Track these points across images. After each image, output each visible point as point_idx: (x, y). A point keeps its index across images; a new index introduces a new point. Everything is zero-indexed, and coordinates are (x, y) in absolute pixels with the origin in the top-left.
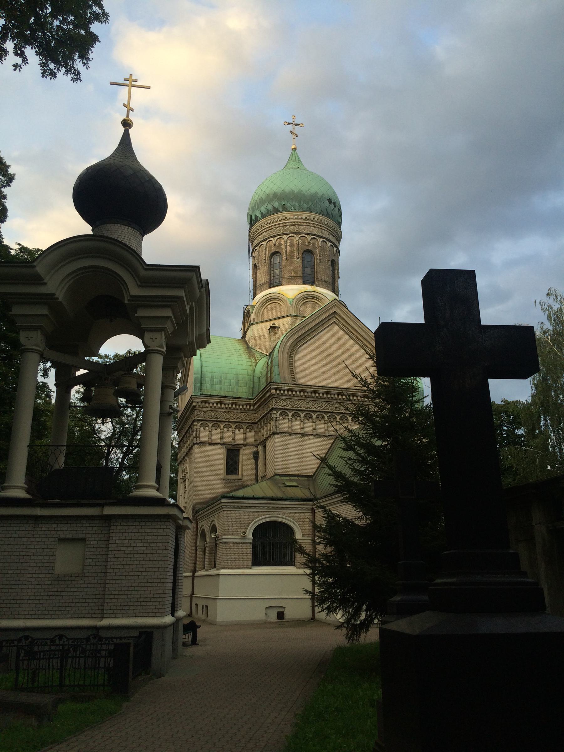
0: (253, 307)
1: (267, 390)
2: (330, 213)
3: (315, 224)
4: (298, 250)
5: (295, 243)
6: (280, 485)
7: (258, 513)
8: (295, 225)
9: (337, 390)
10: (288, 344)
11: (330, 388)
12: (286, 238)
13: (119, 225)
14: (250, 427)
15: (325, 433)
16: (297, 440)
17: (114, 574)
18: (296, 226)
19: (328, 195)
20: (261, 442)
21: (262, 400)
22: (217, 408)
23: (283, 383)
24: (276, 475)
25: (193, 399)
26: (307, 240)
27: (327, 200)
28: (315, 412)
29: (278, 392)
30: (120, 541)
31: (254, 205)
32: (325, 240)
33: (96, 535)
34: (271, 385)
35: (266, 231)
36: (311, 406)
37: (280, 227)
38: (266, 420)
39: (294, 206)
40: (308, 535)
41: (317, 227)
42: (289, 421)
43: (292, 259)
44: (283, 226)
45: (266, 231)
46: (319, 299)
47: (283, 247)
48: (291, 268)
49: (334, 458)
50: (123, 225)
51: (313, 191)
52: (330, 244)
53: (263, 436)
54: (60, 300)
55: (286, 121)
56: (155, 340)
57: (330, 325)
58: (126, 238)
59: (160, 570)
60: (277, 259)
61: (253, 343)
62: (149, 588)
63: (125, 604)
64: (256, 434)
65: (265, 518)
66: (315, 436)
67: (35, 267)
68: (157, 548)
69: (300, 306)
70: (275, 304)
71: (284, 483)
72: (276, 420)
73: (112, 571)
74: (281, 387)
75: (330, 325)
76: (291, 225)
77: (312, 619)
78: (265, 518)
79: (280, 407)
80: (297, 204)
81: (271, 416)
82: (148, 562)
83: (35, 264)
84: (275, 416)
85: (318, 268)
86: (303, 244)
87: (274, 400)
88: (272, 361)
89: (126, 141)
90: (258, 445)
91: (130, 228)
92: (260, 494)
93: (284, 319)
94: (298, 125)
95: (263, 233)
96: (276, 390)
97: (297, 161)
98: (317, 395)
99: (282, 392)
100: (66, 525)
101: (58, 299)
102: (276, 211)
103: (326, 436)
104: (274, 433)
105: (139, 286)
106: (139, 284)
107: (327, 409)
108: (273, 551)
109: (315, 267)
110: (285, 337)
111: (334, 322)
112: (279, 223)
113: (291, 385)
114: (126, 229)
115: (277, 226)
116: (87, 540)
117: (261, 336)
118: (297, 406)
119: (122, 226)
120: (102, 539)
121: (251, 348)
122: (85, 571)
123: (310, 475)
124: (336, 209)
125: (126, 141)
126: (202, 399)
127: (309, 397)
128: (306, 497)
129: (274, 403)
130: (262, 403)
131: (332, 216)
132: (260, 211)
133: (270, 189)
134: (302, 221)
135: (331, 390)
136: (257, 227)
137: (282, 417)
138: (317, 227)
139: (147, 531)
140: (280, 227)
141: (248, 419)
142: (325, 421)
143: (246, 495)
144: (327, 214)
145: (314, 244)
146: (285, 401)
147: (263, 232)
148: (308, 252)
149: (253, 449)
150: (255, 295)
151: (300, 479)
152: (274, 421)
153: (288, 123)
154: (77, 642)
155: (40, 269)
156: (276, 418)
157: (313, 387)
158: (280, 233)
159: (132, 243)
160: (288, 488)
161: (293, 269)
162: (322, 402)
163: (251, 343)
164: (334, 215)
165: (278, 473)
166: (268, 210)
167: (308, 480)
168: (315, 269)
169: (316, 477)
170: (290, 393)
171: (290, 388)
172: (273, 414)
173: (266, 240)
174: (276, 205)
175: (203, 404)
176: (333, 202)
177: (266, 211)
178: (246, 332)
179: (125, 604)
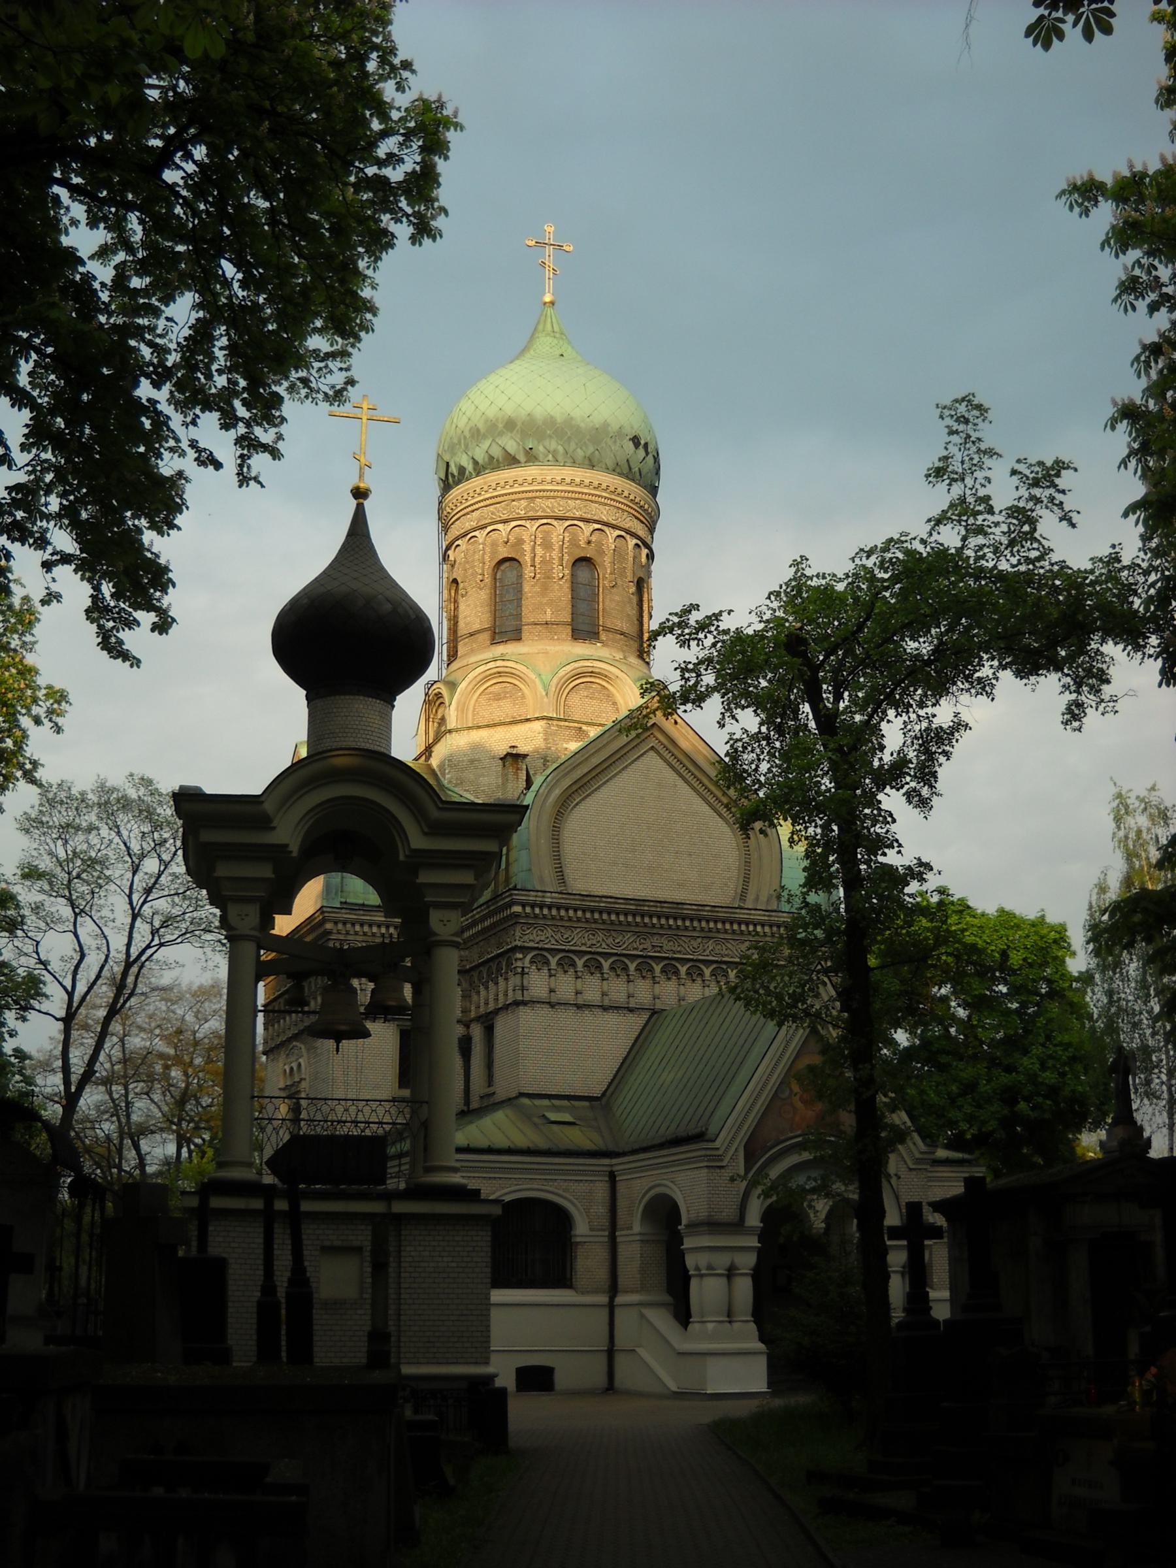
3: (602, 497)
4: (561, 559)
5: (554, 540)
6: (536, 1120)
8: (554, 498)
9: (656, 907)
11: (641, 903)
12: (535, 528)
13: (361, 698)
15: (628, 1003)
16: (567, 1017)
18: (558, 499)
20: (480, 1017)
21: (487, 923)
22: (370, 934)
24: (522, 1095)
25: (326, 915)
26: (583, 533)
28: (606, 955)
29: (528, 910)
31: (456, 441)
32: (623, 533)
34: (511, 895)
35: (486, 506)
36: (601, 942)
37: (520, 499)
39: (555, 454)
41: (606, 504)
42: (550, 976)
43: (549, 578)
44: (527, 498)
45: (486, 506)
46: (610, 678)
47: (527, 547)
48: (545, 600)
49: (649, 1064)
50: (369, 696)
51: (597, 420)
52: (635, 541)
57: (642, 755)
61: (452, 778)
65: (515, 1191)
66: (605, 1009)
67: (263, 802)
69: (564, 696)
71: (544, 1116)
72: (523, 973)
75: (642, 755)
76: (548, 498)
78: (515, 1191)
79: (531, 944)
80: (560, 449)
81: (509, 964)
84: (519, 964)
85: (607, 603)
86: (574, 543)
87: (518, 928)
89: (358, 530)
92: (501, 1142)
93: (528, 725)
95: (477, 509)
96: (524, 906)
97: (558, 335)
98: (613, 917)
99: (537, 911)
101: (291, 852)
102: (511, 461)
103: (631, 1010)
104: (517, 1003)
105: (425, 834)
106: (426, 830)
107: (635, 949)
109: (601, 600)
110: (545, 784)
111: (652, 748)
112: (517, 490)
113: (557, 895)
115: (513, 497)
117: (472, 761)
125: (358, 530)
127: (595, 921)
129: (518, 934)
131: (640, 475)
133: (498, 409)
134: (571, 489)
138: (606, 504)
139: (457, 1238)
140: (520, 499)
142: (628, 975)
144: (628, 472)
145: (599, 544)
147: (477, 506)
148: (583, 562)
151: (574, 1106)
152: (518, 977)
155: (268, 807)
156: (523, 968)
157: (604, 899)
158: (519, 514)
160: (555, 1127)
161: (551, 603)
163: (447, 776)
164: (643, 473)
166: (491, 458)
167: (592, 1107)
168: (601, 604)
170: (554, 912)
171: (554, 900)
172: (516, 960)
174: (512, 446)
175: (349, 926)
176: (642, 442)
177: (486, 459)
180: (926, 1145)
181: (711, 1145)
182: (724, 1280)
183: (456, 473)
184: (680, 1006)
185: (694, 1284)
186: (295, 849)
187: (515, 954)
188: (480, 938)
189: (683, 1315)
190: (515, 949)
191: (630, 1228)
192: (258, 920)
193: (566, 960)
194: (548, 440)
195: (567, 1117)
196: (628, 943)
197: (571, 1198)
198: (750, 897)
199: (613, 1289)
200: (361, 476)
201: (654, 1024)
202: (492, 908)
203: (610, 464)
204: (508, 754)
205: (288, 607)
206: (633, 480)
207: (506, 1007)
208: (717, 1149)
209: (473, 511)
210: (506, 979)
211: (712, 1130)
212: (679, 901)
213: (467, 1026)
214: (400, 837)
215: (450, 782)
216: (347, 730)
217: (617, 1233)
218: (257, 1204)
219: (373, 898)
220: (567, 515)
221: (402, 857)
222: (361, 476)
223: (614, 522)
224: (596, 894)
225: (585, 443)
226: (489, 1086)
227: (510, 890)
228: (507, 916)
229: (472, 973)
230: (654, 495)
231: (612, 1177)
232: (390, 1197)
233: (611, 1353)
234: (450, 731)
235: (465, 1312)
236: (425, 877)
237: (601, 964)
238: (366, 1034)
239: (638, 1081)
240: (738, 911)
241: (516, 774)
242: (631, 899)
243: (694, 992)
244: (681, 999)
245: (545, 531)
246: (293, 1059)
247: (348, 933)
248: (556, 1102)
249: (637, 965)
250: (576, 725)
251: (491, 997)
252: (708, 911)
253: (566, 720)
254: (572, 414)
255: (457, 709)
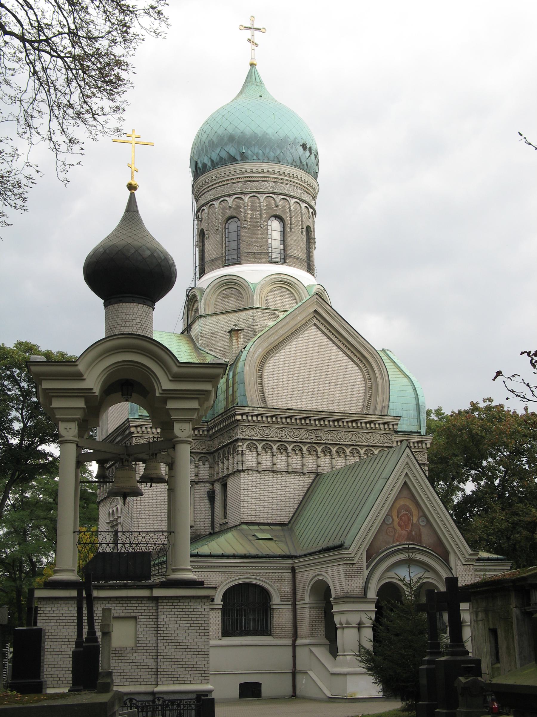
0: (202, 291)
1: (228, 415)
2: (305, 163)
7: (229, 574)
9: (318, 414)
10: (256, 355)
13: (135, 304)
14: (203, 458)
15: (303, 469)
16: (268, 478)
17: (164, 648)
19: (302, 138)
20: (220, 479)
21: (222, 426)
23: (251, 406)
24: (242, 523)
25: (130, 423)
27: (301, 145)
30: (168, 619)
31: (200, 148)
33: (145, 614)
35: (219, 187)
38: (226, 451)
40: (287, 599)
41: (287, 184)
44: (242, 182)
45: (219, 187)
53: (223, 472)
54: (97, 394)
55: (242, 24)
56: (184, 430)
58: (141, 317)
59: (203, 643)
60: (233, 226)
62: (195, 660)
63: (176, 673)
64: (211, 467)
67: (77, 365)
68: (200, 625)
70: (231, 289)
71: (255, 535)
73: (162, 644)
74: (248, 411)
77: (293, 696)
79: (247, 437)
80: (260, 152)
82: (193, 637)
83: (77, 363)
84: (240, 448)
87: (239, 428)
88: (234, 376)
90: (215, 481)
91: (144, 306)
92: (229, 551)
93: (245, 312)
94: (259, 29)
95: (214, 188)
100: (119, 605)
103: (303, 473)
104: (239, 471)
105: (171, 381)
106: (171, 379)
108: (234, 616)
113: (261, 409)
114: (141, 307)
115: (235, 181)
116: (138, 618)
117: (213, 333)
118: (268, 435)
119: (137, 304)
120: (151, 617)
121: (199, 349)
122: (138, 645)
123: (285, 523)
124: (313, 157)
126: (142, 423)
128: (284, 554)
130: (221, 429)
132: (210, 158)
135: (311, 414)
136: (206, 178)
137: (249, 450)
139: (190, 610)
141: (201, 448)
142: (302, 454)
143: (214, 552)
146: (253, 430)
147: (214, 187)
149: (208, 486)
150: (202, 273)
153: (245, 27)
154: (145, 704)
155: (81, 367)
157: (288, 411)
159: (147, 321)
162: (300, 430)
163: (200, 342)
164: (309, 165)
165: (245, 521)
166: (221, 158)
167: (283, 530)
169: (292, 527)
171: (259, 412)
172: (239, 446)
173: (219, 199)
176: (308, 147)
177: (218, 159)
178: (192, 325)
179: (176, 673)
180: (472, 550)
181: (346, 551)
182: (356, 630)
183: (201, 168)
184: (332, 470)
185: (339, 632)
186: (97, 391)
187: (237, 443)
188: (219, 434)
189: (334, 651)
190: (237, 440)
191: (304, 600)
192: (76, 431)
193: (267, 446)
194: (253, 147)
195: (268, 536)
196: (302, 435)
197: (270, 583)
198: (372, 408)
199: (295, 636)
200: (132, 177)
201: (318, 481)
202: (225, 417)
203: (290, 161)
204: (232, 330)
205: (92, 253)
206: (303, 169)
207: (234, 473)
208: (350, 553)
209: (211, 190)
210: (233, 457)
211: (347, 543)
212: (331, 411)
213: (213, 484)
214: (157, 384)
215: (201, 345)
216: (127, 323)
217: (297, 603)
218: (74, 593)
219: (148, 415)
220: (265, 191)
221: (158, 394)
222: (132, 177)
223: (292, 194)
224: (284, 408)
225: (274, 148)
226: (225, 518)
227: (234, 406)
228: (233, 422)
229: (215, 454)
230: (316, 178)
231: (293, 570)
232: (151, 587)
233: (294, 673)
234: (201, 317)
235: (195, 653)
236: (171, 405)
237: (287, 447)
238: (139, 494)
239: (308, 514)
240: (365, 416)
241: (237, 340)
242: (303, 410)
243: (340, 462)
244: (332, 467)
245: (252, 200)
246: (114, 505)
247: (143, 433)
248: (262, 527)
249: (308, 448)
250: (272, 311)
251: (225, 468)
252: (347, 416)
253: (266, 309)
254: (266, 131)
255: (205, 304)
